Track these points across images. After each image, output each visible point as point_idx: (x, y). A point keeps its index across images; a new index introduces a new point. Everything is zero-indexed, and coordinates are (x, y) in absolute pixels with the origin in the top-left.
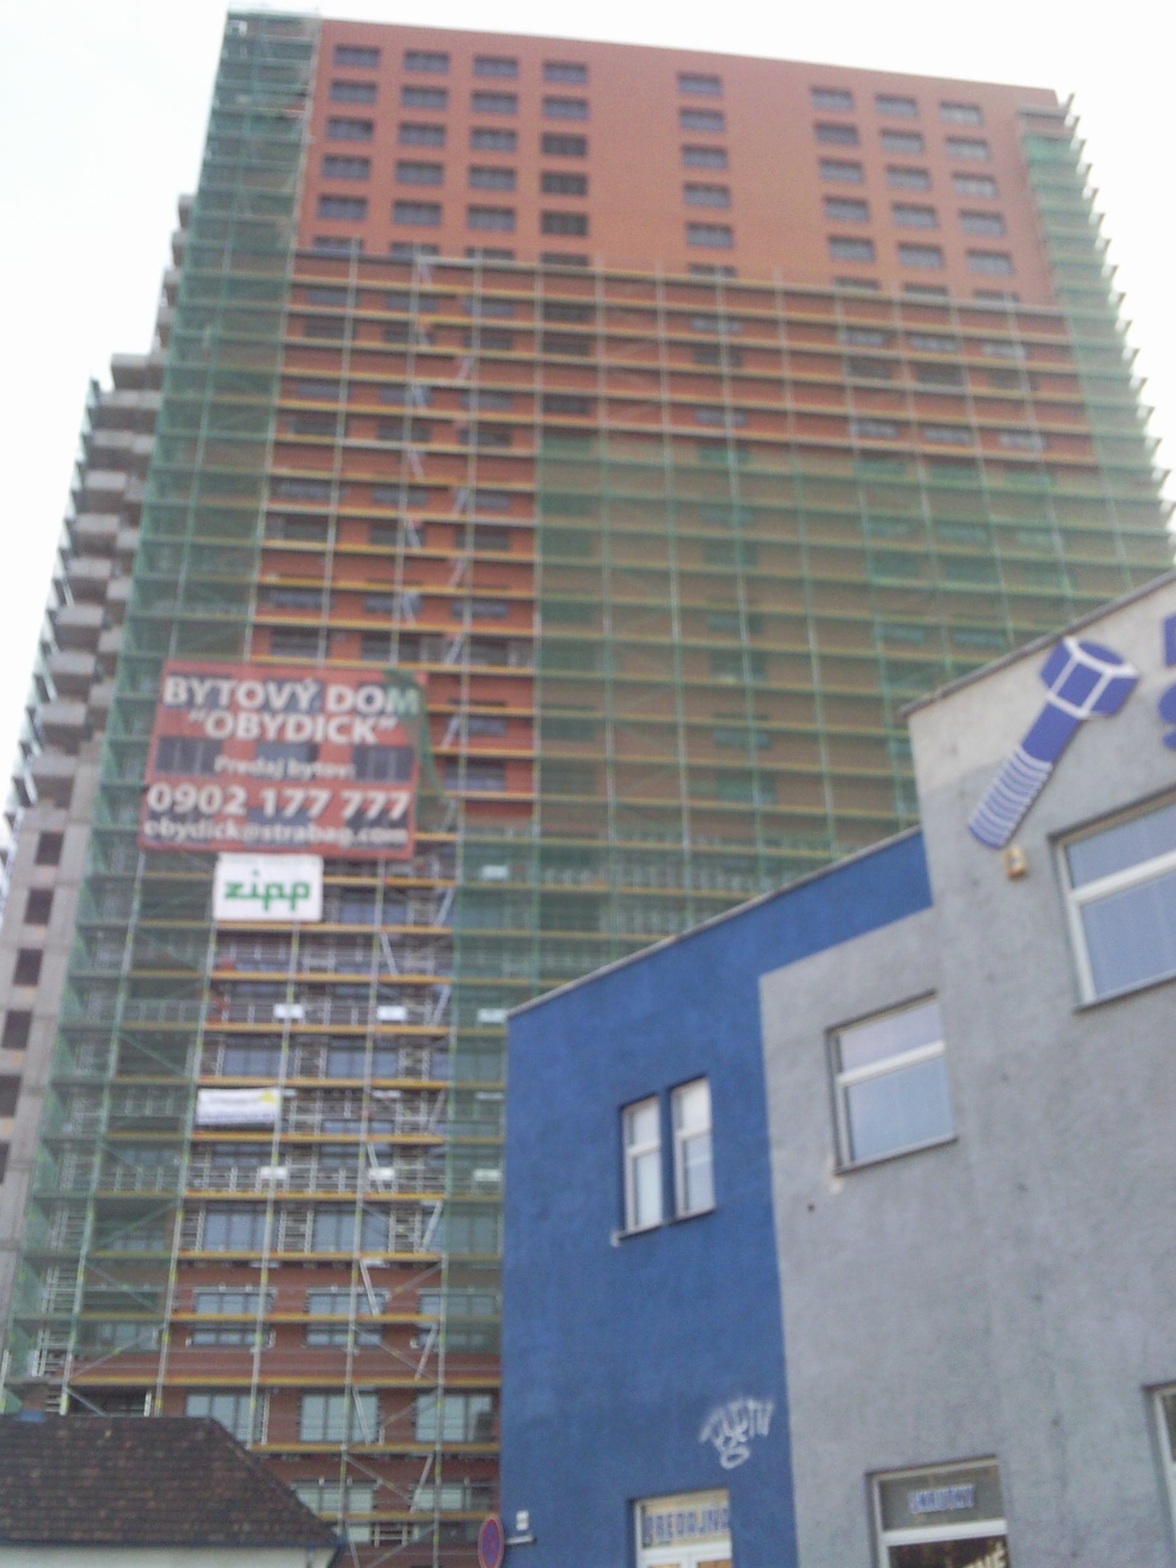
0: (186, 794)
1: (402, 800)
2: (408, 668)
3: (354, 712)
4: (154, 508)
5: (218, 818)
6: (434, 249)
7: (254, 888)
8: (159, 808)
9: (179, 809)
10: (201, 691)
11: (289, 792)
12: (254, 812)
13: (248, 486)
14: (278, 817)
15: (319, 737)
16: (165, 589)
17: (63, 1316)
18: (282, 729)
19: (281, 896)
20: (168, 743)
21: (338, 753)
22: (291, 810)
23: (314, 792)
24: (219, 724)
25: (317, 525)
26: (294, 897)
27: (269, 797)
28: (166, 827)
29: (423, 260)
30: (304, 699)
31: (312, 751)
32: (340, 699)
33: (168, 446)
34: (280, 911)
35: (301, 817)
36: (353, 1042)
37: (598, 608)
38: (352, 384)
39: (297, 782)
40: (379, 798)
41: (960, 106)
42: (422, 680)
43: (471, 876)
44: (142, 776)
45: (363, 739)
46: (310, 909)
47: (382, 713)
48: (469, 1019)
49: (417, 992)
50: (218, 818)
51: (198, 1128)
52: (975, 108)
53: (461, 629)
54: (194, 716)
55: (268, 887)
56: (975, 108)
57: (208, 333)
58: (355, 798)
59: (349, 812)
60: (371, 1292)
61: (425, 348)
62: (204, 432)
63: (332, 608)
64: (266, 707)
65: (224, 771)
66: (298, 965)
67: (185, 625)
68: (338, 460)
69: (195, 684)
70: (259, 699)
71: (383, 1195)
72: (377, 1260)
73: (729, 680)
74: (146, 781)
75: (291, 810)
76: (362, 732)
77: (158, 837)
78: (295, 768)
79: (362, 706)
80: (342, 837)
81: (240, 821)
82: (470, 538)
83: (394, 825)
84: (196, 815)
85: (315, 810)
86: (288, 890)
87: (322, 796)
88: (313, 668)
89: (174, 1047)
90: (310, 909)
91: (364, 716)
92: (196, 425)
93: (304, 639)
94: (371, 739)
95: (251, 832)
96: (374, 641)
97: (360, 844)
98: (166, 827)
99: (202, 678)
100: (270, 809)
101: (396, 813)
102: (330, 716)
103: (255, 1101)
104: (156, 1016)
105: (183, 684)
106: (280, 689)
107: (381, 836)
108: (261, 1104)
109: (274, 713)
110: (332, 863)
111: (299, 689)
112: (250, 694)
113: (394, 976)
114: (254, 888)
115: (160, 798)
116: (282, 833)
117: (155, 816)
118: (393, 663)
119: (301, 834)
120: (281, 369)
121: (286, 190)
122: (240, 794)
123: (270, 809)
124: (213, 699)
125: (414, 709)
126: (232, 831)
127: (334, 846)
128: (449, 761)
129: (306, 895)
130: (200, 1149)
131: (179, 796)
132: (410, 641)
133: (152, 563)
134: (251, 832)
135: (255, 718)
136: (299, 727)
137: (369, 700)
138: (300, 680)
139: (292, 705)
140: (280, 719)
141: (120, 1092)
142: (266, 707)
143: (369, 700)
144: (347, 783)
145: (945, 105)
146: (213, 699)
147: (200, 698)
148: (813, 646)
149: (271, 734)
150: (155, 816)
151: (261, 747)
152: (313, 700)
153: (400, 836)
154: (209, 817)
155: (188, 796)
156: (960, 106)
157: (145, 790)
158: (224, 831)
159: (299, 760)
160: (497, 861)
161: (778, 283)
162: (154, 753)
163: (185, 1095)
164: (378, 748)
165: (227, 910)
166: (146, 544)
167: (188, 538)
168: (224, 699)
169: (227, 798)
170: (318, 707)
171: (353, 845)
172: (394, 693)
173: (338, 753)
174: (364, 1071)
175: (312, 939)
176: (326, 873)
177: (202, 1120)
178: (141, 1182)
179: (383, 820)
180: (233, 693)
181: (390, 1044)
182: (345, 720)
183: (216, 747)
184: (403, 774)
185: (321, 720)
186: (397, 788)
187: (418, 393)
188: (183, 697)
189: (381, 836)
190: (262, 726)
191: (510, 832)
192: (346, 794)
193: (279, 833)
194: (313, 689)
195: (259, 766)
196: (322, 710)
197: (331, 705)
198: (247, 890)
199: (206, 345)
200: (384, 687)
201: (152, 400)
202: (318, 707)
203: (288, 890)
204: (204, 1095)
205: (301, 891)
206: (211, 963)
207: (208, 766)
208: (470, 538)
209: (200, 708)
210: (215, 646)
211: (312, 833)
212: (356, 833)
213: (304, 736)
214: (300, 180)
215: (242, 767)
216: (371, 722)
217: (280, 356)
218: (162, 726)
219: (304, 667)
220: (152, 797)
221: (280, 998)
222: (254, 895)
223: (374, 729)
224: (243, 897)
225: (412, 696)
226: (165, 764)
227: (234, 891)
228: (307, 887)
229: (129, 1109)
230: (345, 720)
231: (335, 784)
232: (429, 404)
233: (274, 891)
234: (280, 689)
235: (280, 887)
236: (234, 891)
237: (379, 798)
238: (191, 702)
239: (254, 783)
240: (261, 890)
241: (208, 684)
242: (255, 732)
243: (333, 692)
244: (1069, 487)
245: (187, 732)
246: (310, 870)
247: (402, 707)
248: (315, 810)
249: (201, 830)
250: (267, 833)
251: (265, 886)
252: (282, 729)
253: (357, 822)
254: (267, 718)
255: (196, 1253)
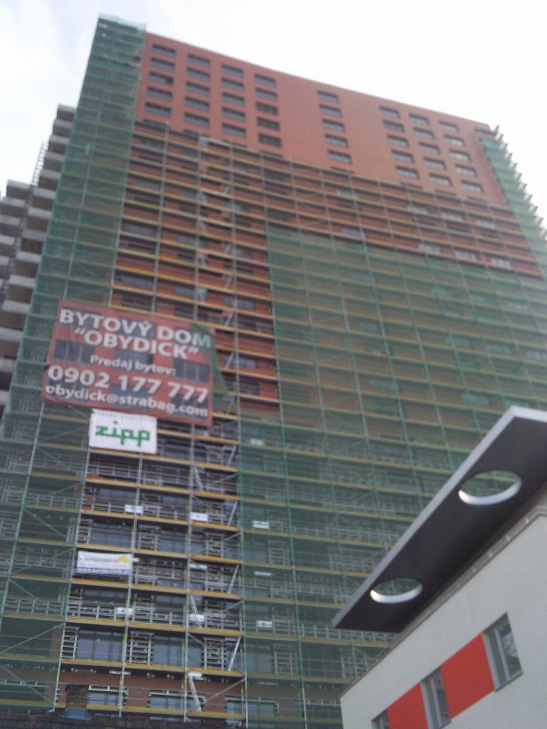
0: (72, 373)
1: (204, 393)
2: (202, 324)
3: (174, 341)
4: (54, 224)
5: (92, 388)
6: (207, 136)
7: (115, 430)
8: (54, 378)
9: (67, 381)
10: (82, 320)
11: (135, 378)
12: (114, 387)
13: (67, 488)
14: (129, 391)
15: (153, 351)
16: (62, 265)
17: (8, 539)
18: (131, 344)
19: (132, 437)
20: (61, 344)
21: (165, 362)
22: (137, 388)
23: (151, 380)
24: (93, 337)
25: (150, 246)
26: (140, 439)
27: (124, 379)
28: (58, 390)
29: (202, 139)
30: (144, 331)
31: (150, 358)
32: (165, 333)
33: (62, 195)
34: (131, 445)
35: (144, 392)
36: (172, 638)
37: (312, 368)
38: (160, 280)
39: (140, 373)
40: (190, 390)
41: (448, 124)
42: (213, 332)
43: (251, 629)
44: (45, 361)
45: (180, 355)
46: (150, 446)
47: (190, 344)
48: (249, 525)
49: (216, 503)
50: (92, 388)
51: (78, 576)
52: (454, 126)
53: (232, 309)
54: (77, 331)
55: (123, 431)
56: (454, 126)
57: (88, 148)
58: (176, 387)
59: (173, 394)
60: (196, 697)
61: (205, 176)
62: (85, 192)
63: (161, 252)
64: (121, 332)
65: (96, 362)
66: (143, 482)
67: (71, 283)
68: (160, 217)
69: (79, 314)
70: (117, 327)
71: (200, 630)
72: (197, 675)
73: (377, 354)
74: (48, 363)
75: (137, 388)
76: (179, 352)
77: (54, 394)
78: (139, 365)
79: (178, 338)
80: (170, 409)
81: (104, 391)
82: (237, 384)
83: (200, 406)
84: (78, 385)
85: (152, 390)
86: (136, 434)
87: (157, 383)
88: (149, 316)
89: (61, 522)
90: (150, 446)
91: (180, 345)
92: (82, 188)
93: (144, 301)
94: (184, 356)
95: (112, 399)
96: (183, 309)
97: (179, 413)
98: (58, 390)
99: (83, 312)
100: (124, 387)
101: (201, 399)
102: (159, 342)
103: (115, 561)
104: (50, 502)
105: (71, 314)
106: (129, 324)
107: (191, 410)
108: (121, 563)
109: (126, 336)
110: (163, 422)
111: (141, 325)
112: (112, 324)
113: (202, 493)
114: (115, 430)
115: (56, 373)
116: (132, 401)
117: (52, 383)
118: (196, 321)
119: (143, 402)
120: (128, 171)
121: (131, 94)
122: (106, 377)
123: (124, 387)
124: (89, 325)
125: (209, 345)
126: (101, 397)
127: (164, 412)
128: (229, 376)
129: (148, 438)
130: (76, 591)
131: (67, 374)
132: (204, 313)
133: (27, 354)
134: (112, 399)
135: (115, 337)
136: (141, 345)
137: (183, 337)
138: (142, 321)
139: (136, 332)
140: (130, 339)
141: (23, 548)
142: (121, 332)
143: (183, 337)
144: (170, 378)
145: (441, 123)
146: (89, 325)
147: (81, 323)
148: (419, 341)
149: (125, 346)
150: (52, 383)
151: (117, 352)
152: (148, 332)
153: (204, 412)
154: (86, 387)
155: (73, 375)
156: (448, 124)
157: (47, 368)
158: (95, 397)
159: (141, 362)
160: (268, 616)
161: (378, 180)
162: (52, 348)
163: (70, 555)
164: (188, 361)
165: (96, 441)
166: (26, 341)
167: (75, 241)
168: (96, 325)
169: (98, 379)
170: (152, 335)
171: (175, 413)
172: (197, 336)
173: (165, 362)
174: (188, 551)
175: (150, 465)
176: (159, 427)
177: (80, 571)
178: (35, 610)
179: (193, 401)
180: (101, 322)
181: (201, 533)
182: (170, 344)
183: (91, 350)
184: (204, 379)
185: (154, 343)
186: (202, 387)
187: (203, 258)
188: (71, 320)
189: (191, 410)
190: (118, 340)
191: (266, 419)
192: (171, 384)
193: (130, 400)
194: (149, 326)
195: (117, 363)
196: (155, 338)
197: (160, 336)
198: (110, 431)
199: (87, 152)
200: (191, 332)
201: (50, 194)
202: (152, 335)
203: (136, 434)
204: (81, 554)
205: (144, 435)
206: (86, 475)
207: (86, 359)
208: (237, 384)
209: (82, 327)
210: (90, 297)
211: (150, 402)
212: (177, 406)
213: (146, 348)
214: (138, 91)
215: (107, 362)
216: (184, 348)
217: (128, 165)
218: (57, 334)
219: (146, 315)
220: (51, 372)
221: (122, 602)
222: (114, 435)
223: (186, 351)
224: (108, 435)
225: (207, 339)
226: (59, 355)
227: (102, 431)
228: (148, 434)
229: (27, 562)
230: (170, 344)
231: (162, 377)
232: (207, 299)
233: (127, 434)
234: (129, 324)
235: (131, 432)
236: (102, 431)
237: (190, 390)
238: (76, 322)
239: (114, 372)
240: (119, 432)
241: (87, 316)
242: (115, 344)
243: (161, 330)
244: (524, 282)
245: (73, 339)
246: (150, 425)
247: (202, 344)
248: (152, 390)
249: (80, 395)
250: (122, 400)
251: (121, 431)
252: (131, 344)
253: (178, 400)
254: (122, 338)
255: (73, 660)
